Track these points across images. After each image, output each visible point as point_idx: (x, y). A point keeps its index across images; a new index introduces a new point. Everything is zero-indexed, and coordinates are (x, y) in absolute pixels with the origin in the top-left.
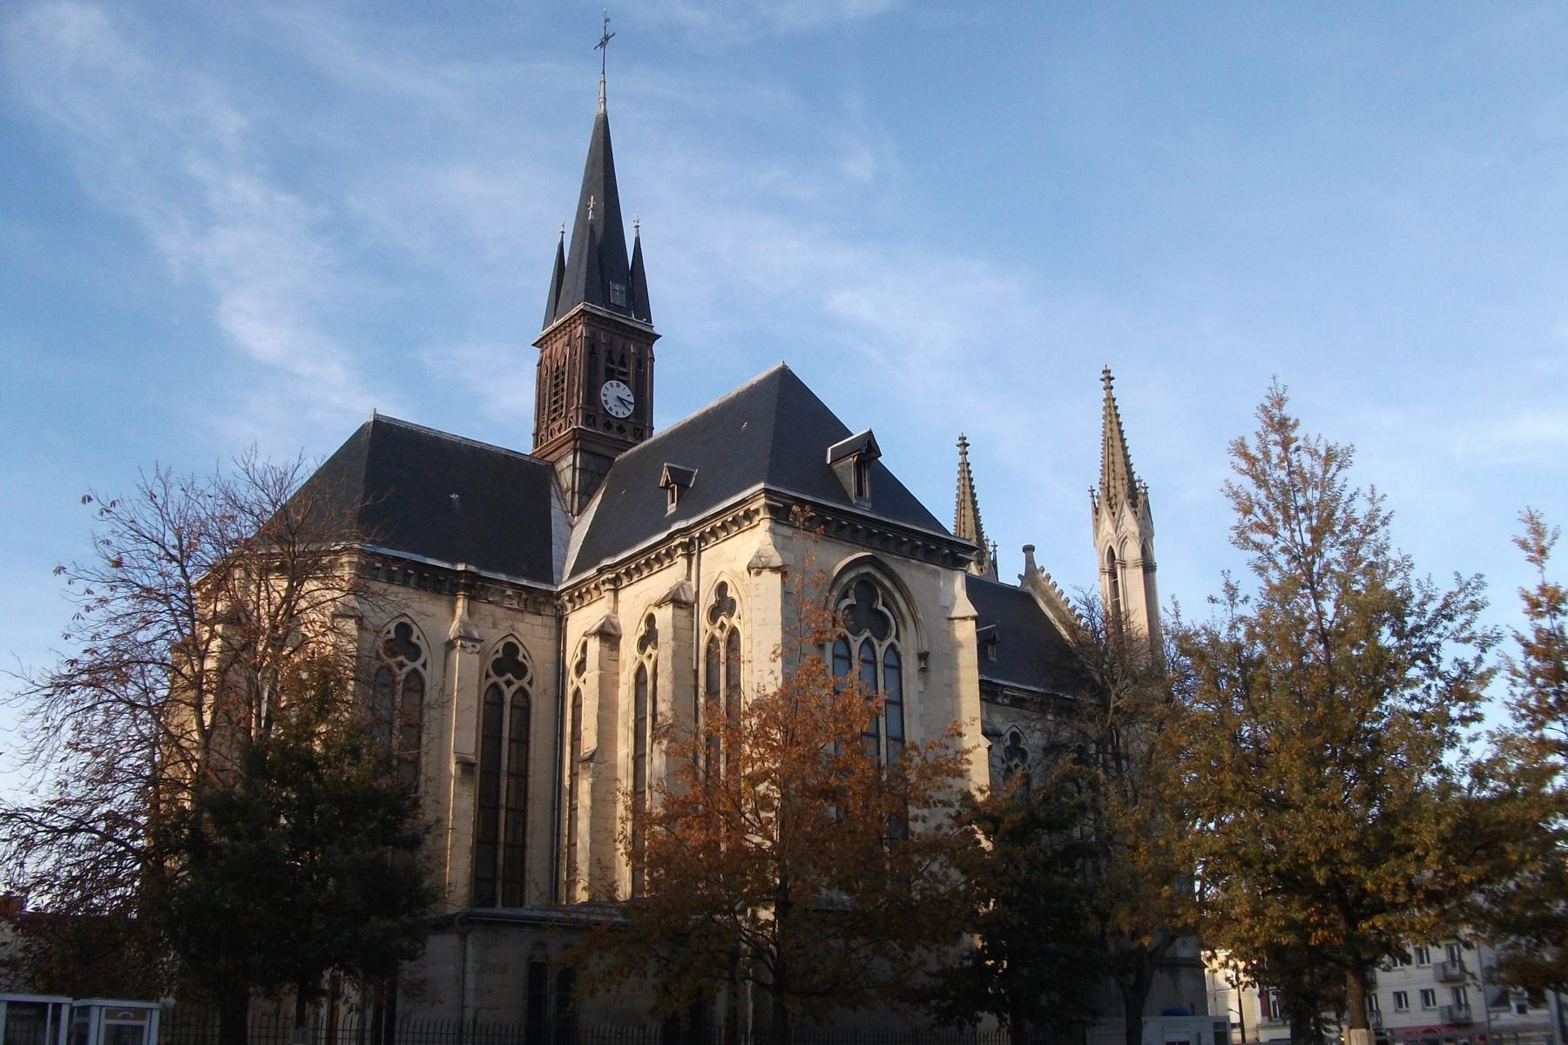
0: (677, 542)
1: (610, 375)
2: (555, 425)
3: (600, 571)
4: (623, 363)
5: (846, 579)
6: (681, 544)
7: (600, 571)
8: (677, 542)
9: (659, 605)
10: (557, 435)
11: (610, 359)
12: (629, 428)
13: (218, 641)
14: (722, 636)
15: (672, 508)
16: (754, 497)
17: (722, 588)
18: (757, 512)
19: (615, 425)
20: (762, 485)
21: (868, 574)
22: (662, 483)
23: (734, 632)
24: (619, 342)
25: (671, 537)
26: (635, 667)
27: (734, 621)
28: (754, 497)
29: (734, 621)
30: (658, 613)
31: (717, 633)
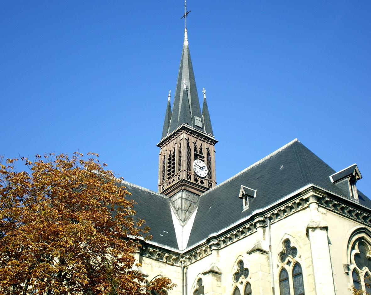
0: (256, 220)
1: (196, 156)
2: (171, 180)
3: (208, 241)
4: (201, 152)
5: (354, 239)
6: (259, 221)
7: (208, 241)
8: (256, 220)
9: (205, 274)
10: (171, 185)
11: (195, 150)
12: (205, 182)
13: (105, 264)
14: (290, 269)
15: (246, 208)
16: (306, 191)
17: (287, 242)
18: (307, 200)
19: (199, 180)
20: (310, 185)
21: (363, 238)
22: (240, 196)
23: (297, 265)
24: (199, 143)
25: (252, 219)
26: (277, 272)
27: (297, 259)
28: (306, 191)
29: (297, 259)
30: (204, 278)
31: (287, 267)
